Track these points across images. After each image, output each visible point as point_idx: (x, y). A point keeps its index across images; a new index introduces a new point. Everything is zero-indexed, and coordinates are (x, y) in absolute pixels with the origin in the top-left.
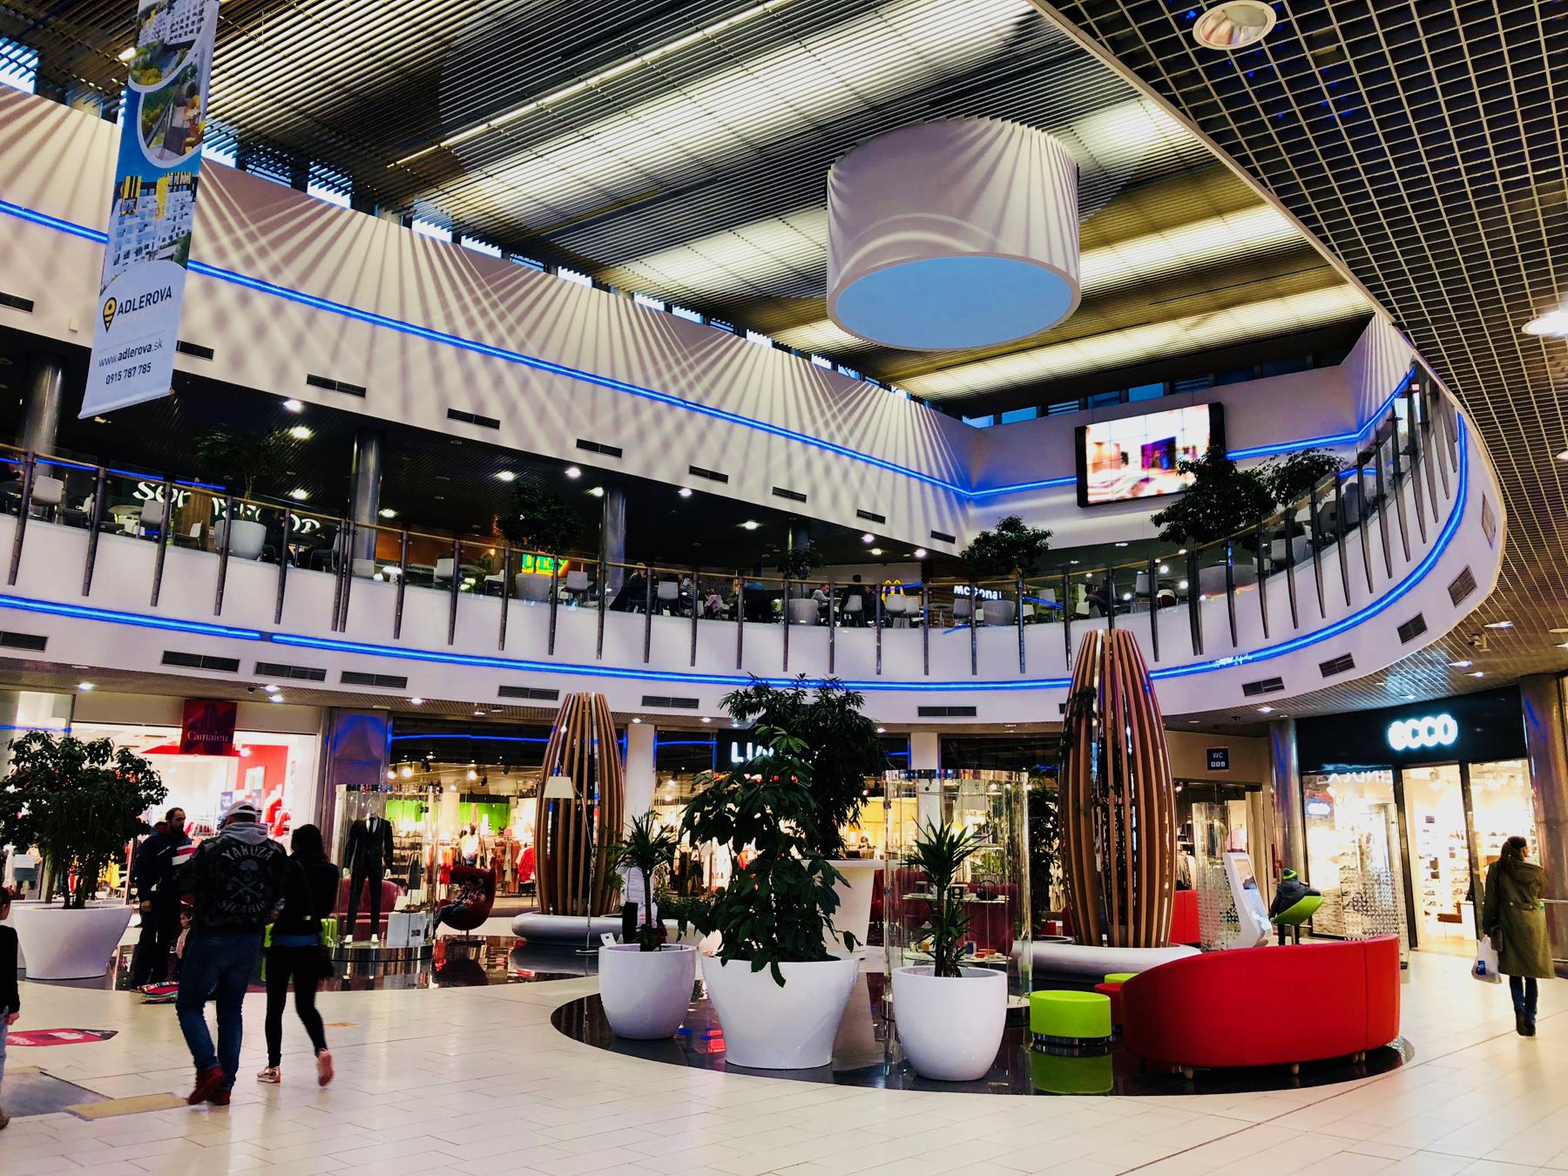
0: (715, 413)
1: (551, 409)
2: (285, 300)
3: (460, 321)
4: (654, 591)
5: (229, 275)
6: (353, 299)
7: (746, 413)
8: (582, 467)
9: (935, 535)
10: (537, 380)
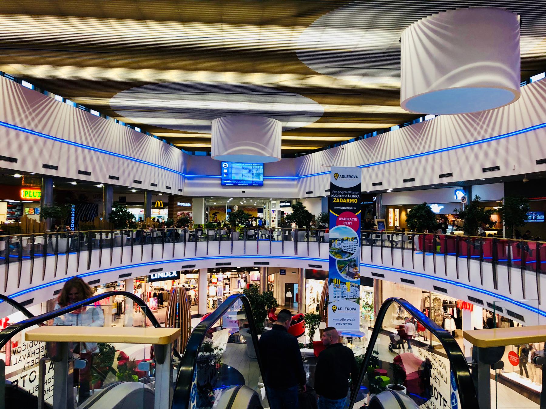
0: (140, 161)
1: (104, 166)
2: (21, 132)
3: (18, 120)
4: (417, 235)
5: (23, 130)
6: (56, 135)
7: (53, 134)
8: (77, 181)
9: (80, 172)
10: (101, 156)
